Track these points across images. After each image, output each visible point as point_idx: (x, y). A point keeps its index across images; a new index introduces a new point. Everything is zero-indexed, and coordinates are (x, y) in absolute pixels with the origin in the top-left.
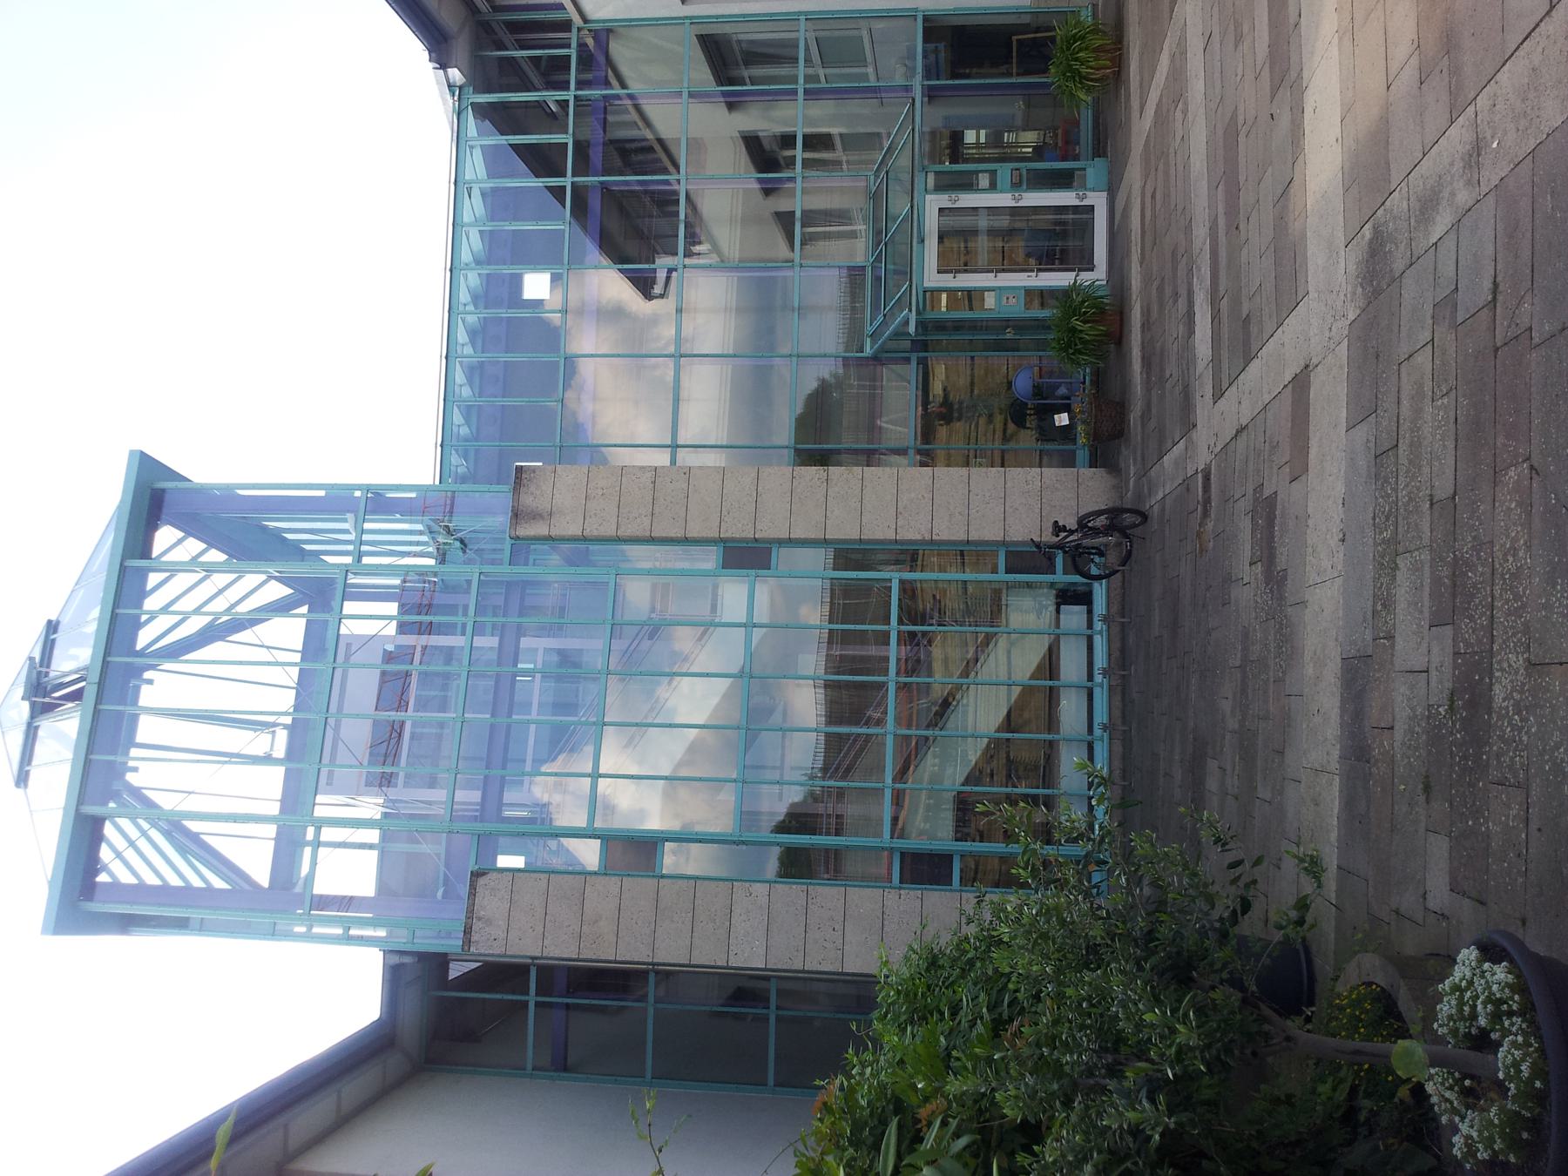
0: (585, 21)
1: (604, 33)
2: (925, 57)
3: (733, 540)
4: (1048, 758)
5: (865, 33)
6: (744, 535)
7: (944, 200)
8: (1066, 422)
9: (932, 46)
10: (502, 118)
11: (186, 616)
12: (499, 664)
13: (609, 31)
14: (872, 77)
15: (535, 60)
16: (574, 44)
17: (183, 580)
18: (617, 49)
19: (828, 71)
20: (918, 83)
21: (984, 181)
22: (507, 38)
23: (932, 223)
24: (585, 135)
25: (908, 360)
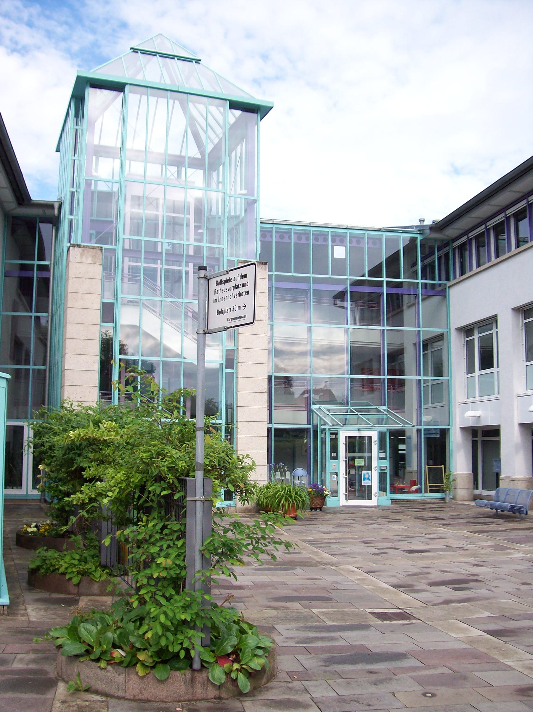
0: (449, 287)
1: (443, 293)
2: (435, 429)
3: (238, 353)
4: (372, 238)
5: (444, 403)
6: (239, 358)
7: (375, 438)
8: (354, 473)
9: (439, 432)
10: (410, 247)
11: (206, 120)
12: (186, 256)
13: (445, 297)
14: (427, 406)
15: (434, 262)
16: (440, 282)
17: (220, 118)
18: (435, 300)
19: (430, 387)
20: (422, 427)
21: (382, 455)
22: (442, 253)
23: (365, 433)
24: (405, 286)
25: (309, 423)
